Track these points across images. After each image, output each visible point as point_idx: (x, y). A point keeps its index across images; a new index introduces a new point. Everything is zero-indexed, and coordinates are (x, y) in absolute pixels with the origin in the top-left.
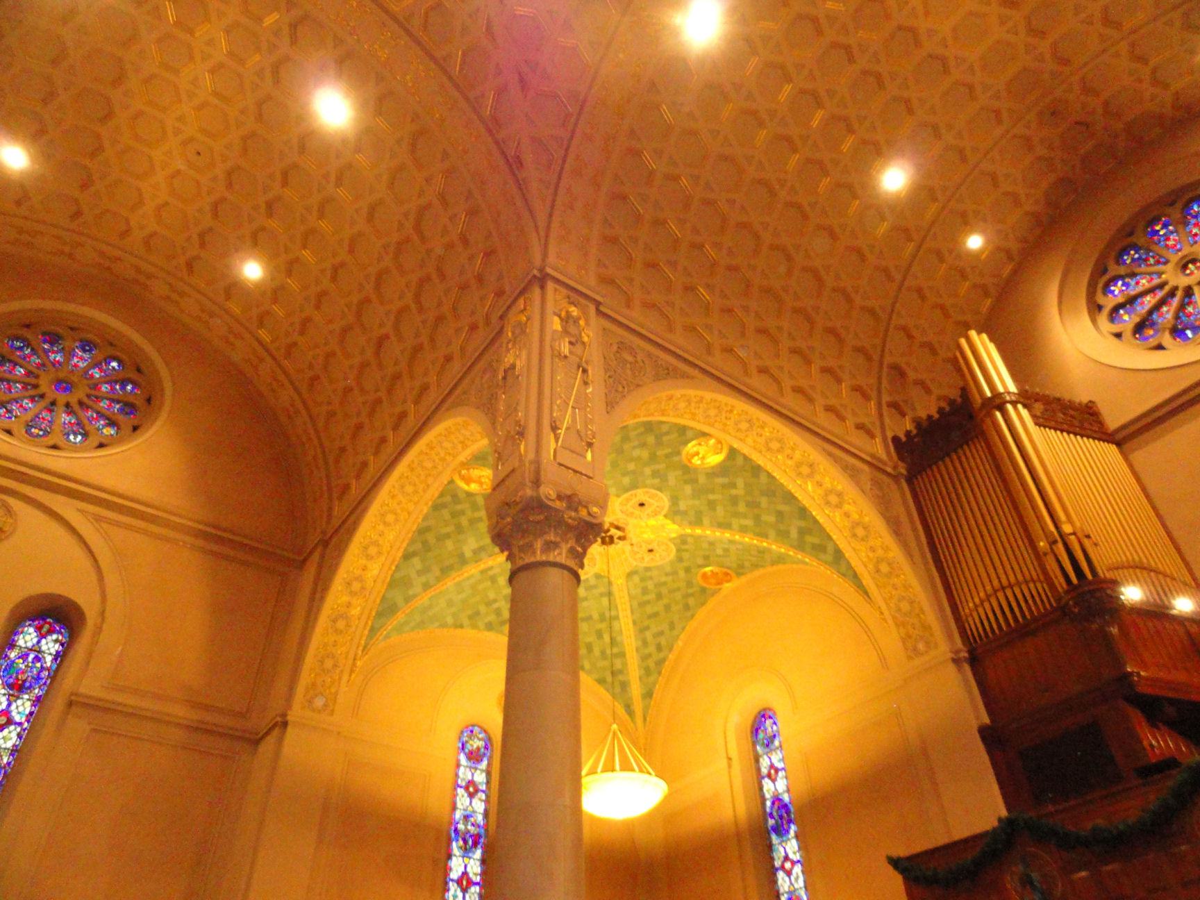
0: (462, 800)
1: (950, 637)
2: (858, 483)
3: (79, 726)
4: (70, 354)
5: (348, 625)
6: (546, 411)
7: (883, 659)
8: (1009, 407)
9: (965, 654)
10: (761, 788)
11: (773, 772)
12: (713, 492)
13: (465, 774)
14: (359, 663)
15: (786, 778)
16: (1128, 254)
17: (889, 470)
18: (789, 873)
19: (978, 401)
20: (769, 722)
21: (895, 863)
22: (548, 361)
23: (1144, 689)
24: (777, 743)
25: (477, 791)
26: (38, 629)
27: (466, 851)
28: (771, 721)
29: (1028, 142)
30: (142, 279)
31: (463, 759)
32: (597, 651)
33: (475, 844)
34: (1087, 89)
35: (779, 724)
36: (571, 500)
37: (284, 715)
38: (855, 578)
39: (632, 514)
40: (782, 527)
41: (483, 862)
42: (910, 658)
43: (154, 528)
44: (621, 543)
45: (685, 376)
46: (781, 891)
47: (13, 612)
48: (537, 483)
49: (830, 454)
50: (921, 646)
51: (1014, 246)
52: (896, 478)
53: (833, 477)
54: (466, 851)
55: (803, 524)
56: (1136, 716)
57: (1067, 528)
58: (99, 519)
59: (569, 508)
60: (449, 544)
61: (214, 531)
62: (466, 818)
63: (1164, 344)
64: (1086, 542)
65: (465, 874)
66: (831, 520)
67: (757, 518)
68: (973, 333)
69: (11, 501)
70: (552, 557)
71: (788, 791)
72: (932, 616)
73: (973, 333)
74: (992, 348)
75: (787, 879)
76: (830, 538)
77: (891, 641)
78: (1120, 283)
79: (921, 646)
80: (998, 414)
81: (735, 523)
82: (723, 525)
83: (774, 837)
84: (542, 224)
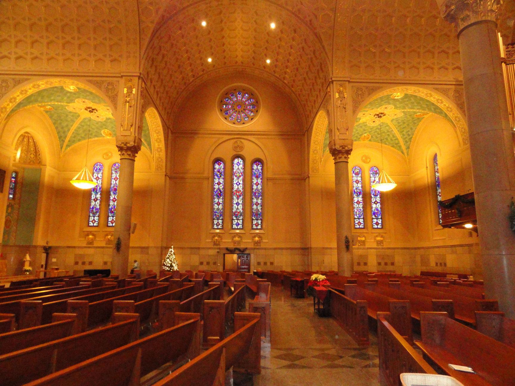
0: (355, 185)
3: (270, 183)
4: (237, 97)
5: (317, 152)
6: (336, 125)
13: (355, 179)
14: (322, 160)
25: (359, 182)
26: (256, 165)
27: (358, 196)
30: (244, 70)
31: (354, 175)
32: (389, 139)
33: (360, 194)
36: (343, 147)
37: (308, 175)
39: (384, 110)
41: (362, 197)
43: (270, 137)
44: (384, 116)
45: (379, 88)
47: (251, 163)
54: (358, 196)
58: (258, 139)
59: (343, 148)
61: (283, 133)
62: (357, 189)
65: (358, 201)
67: (421, 106)
69: (243, 141)
70: (341, 160)
81: (415, 107)
84: (330, 58)
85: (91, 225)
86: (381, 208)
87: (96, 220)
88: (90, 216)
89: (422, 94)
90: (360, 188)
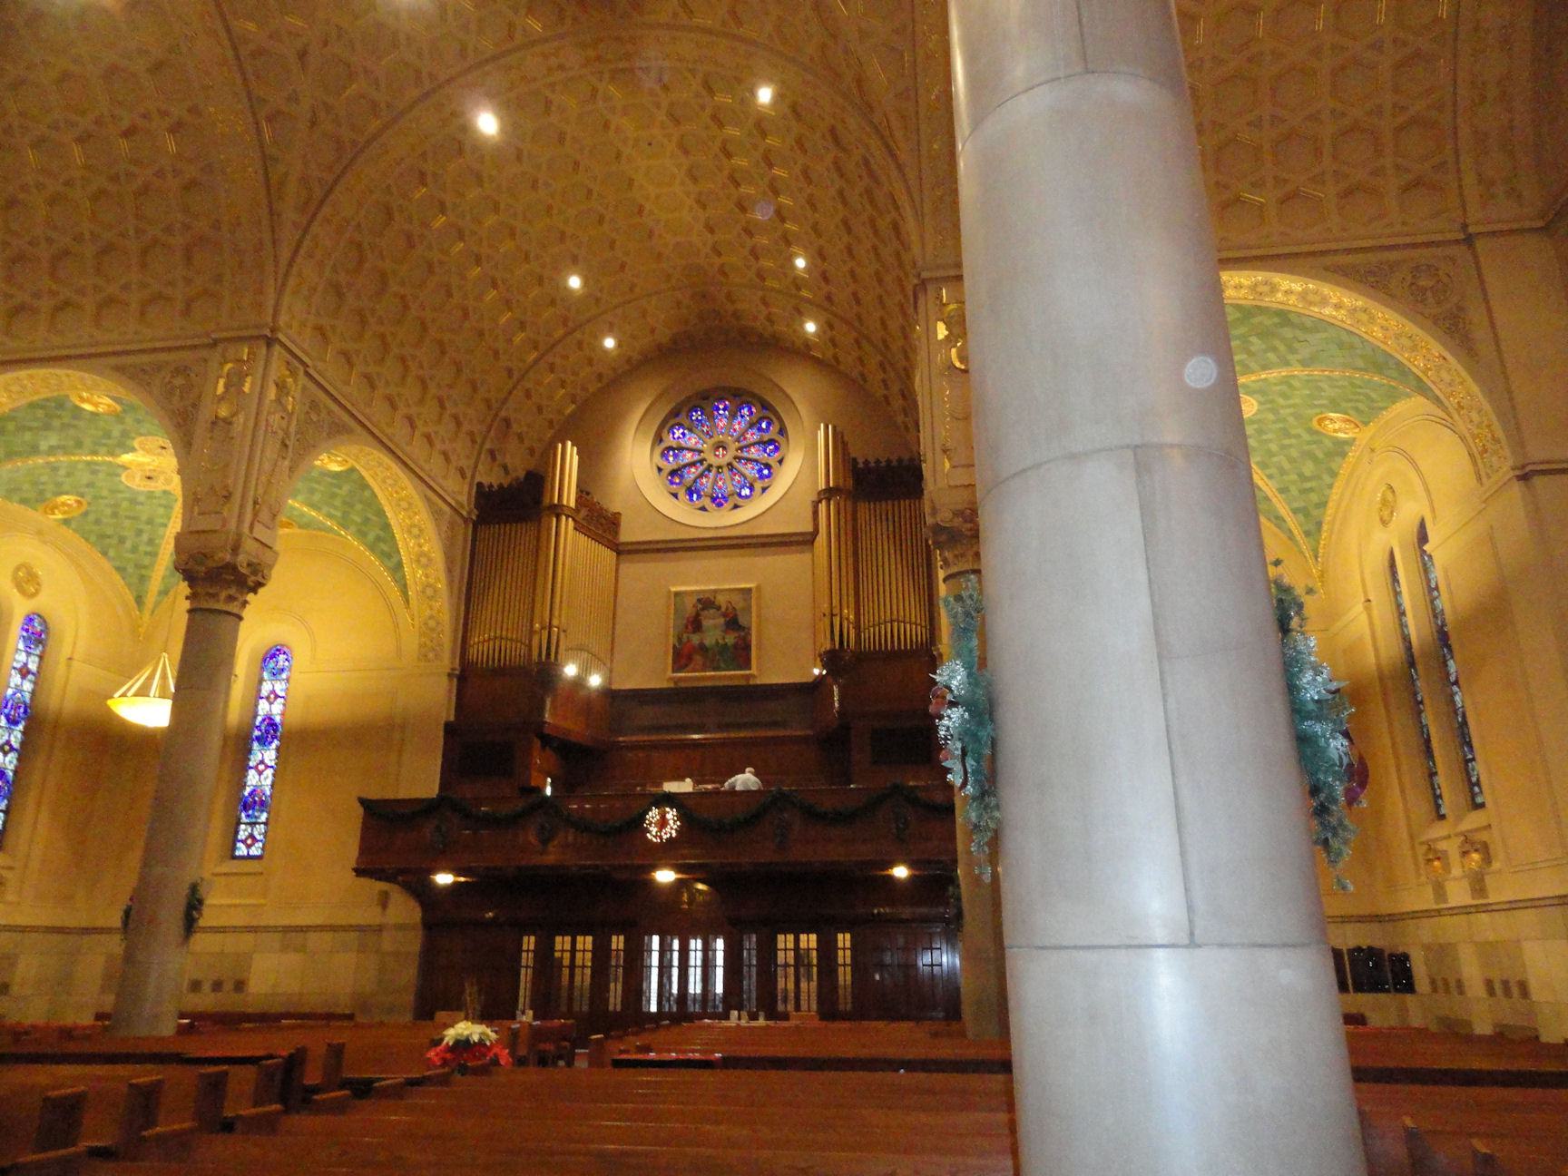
1: (453, 657)
2: (438, 526)
7: (399, 650)
8: (564, 518)
9: (457, 672)
10: (256, 706)
11: (272, 696)
12: (319, 483)
15: (284, 705)
16: (696, 412)
17: (464, 513)
18: (260, 773)
19: (546, 501)
20: (282, 657)
21: (363, 802)
22: (261, 433)
23: (547, 731)
24: (284, 676)
28: (285, 656)
29: (679, 303)
32: (128, 545)
34: (729, 296)
35: (293, 662)
38: (404, 589)
40: (364, 528)
41: (24, 733)
42: (419, 659)
45: (350, 431)
46: (249, 783)
48: (235, 549)
49: (428, 500)
50: (431, 655)
51: (636, 356)
52: (466, 521)
53: (423, 517)
55: (382, 534)
56: (537, 743)
57: (555, 622)
60: (28, 436)
63: (679, 496)
64: (562, 635)
66: (406, 546)
67: (345, 514)
68: (569, 443)
71: (283, 714)
72: (447, 640)
73: (569, 443)
74: (576, 458)
75: (257, 777)
76: (399, 552)
77: (411, 643)
78: (681, 431)
79: (431, 655)
80: (554, 519)
81: (325, 509)
82: (312, 506)
83: (256, 745)
85: (241, 853)
86: (15, 772)
87: (258, 837)
88: (239, 823)
89: (1236, 280)
90: (27, 696)
